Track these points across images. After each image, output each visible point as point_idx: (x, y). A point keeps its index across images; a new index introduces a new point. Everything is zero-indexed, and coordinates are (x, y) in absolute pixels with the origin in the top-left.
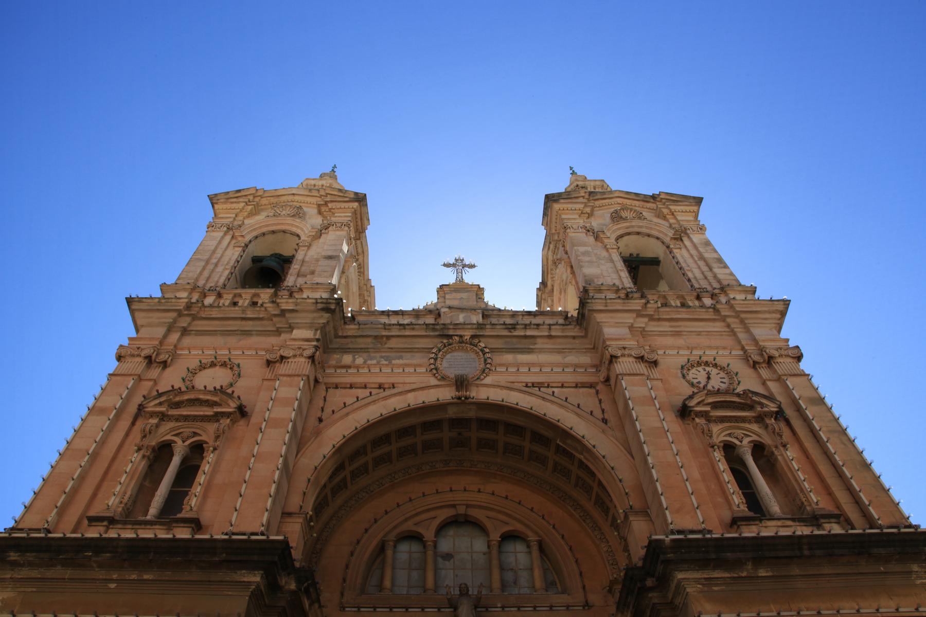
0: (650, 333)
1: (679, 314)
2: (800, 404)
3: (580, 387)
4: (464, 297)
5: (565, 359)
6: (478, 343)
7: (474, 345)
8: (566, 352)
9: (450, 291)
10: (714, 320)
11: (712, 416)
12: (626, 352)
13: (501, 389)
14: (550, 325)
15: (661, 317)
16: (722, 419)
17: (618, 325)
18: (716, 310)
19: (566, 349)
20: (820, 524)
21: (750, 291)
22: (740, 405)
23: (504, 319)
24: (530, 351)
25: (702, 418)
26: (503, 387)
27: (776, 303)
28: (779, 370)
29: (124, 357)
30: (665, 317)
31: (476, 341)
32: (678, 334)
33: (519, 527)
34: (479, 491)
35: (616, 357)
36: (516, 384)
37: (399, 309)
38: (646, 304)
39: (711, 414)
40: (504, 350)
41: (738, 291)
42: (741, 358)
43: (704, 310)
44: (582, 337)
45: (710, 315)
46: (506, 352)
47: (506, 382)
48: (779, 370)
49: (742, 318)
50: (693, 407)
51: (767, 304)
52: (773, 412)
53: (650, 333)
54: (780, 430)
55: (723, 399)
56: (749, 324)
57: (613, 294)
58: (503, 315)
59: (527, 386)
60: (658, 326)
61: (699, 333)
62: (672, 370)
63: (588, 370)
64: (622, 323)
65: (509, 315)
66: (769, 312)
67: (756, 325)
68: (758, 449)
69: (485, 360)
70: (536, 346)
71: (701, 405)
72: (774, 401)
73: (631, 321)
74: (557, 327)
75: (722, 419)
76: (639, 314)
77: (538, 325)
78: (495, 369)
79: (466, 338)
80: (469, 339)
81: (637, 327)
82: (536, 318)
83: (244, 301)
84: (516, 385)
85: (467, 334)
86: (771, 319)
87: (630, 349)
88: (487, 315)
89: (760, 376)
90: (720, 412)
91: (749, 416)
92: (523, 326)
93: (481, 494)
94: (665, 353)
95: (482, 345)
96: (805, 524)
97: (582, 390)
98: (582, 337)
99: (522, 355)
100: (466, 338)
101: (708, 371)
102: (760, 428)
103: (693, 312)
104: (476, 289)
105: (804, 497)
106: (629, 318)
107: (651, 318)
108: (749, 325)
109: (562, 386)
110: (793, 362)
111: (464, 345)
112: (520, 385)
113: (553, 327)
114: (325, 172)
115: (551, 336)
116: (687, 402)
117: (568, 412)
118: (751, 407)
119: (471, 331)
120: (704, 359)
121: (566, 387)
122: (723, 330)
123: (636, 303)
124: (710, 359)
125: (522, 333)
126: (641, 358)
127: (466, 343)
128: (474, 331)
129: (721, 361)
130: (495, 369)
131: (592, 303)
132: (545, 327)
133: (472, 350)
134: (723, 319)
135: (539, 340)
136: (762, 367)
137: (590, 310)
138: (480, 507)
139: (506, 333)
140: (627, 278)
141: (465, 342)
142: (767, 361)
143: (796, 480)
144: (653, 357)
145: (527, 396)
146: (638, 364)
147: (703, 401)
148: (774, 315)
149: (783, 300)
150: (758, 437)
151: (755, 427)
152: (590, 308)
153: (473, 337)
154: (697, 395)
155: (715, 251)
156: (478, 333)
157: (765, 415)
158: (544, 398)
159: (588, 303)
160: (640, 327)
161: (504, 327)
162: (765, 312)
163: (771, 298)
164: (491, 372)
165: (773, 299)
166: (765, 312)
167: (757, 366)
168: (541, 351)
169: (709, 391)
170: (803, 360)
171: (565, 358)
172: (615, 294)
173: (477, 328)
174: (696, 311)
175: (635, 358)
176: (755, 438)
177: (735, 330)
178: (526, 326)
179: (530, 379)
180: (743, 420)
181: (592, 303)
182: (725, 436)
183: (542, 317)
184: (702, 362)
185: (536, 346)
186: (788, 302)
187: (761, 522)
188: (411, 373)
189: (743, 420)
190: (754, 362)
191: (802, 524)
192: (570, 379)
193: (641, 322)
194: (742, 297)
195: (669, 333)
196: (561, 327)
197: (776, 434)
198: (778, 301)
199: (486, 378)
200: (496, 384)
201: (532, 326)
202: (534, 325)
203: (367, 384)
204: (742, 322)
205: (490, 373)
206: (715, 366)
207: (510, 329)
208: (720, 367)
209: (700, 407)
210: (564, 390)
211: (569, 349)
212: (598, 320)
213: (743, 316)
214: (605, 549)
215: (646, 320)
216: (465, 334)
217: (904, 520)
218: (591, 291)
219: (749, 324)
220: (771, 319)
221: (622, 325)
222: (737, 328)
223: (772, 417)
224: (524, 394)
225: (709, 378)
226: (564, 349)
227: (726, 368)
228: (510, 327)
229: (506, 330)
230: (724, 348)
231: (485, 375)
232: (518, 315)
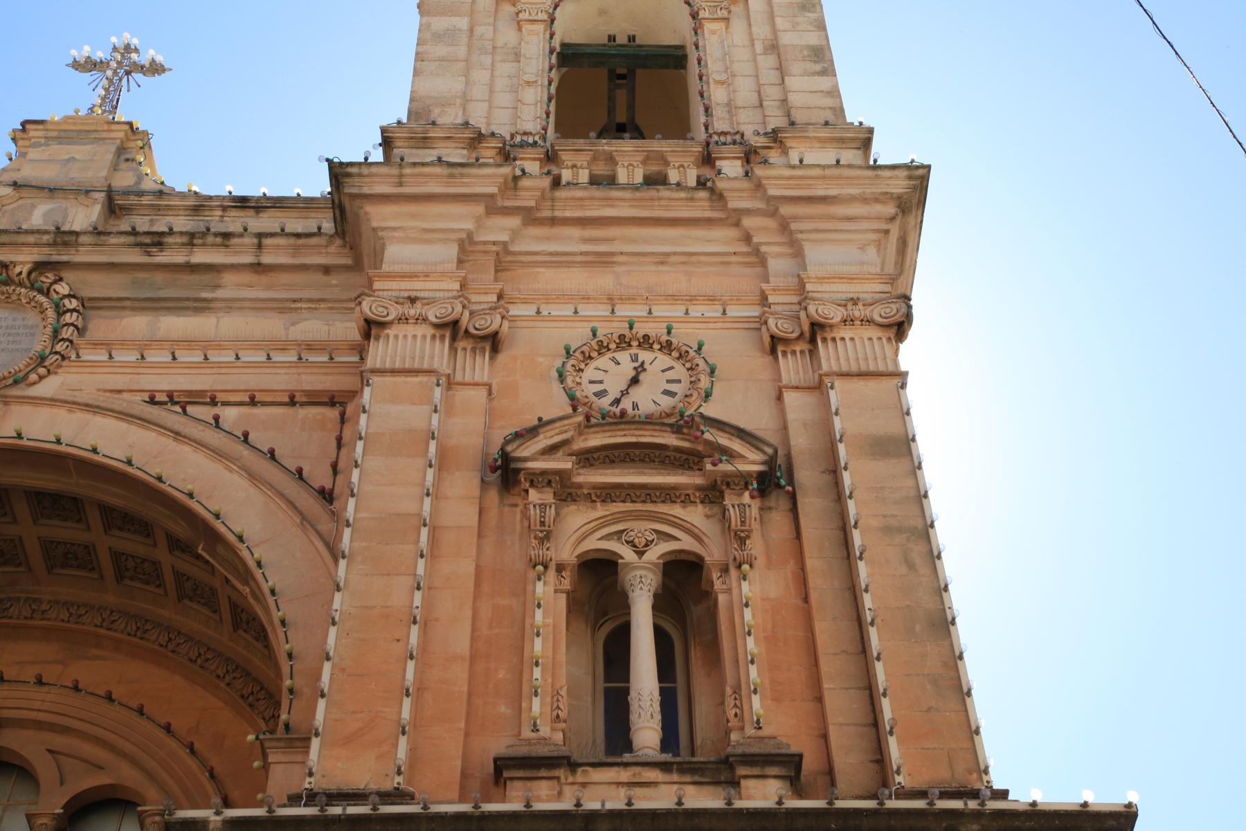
0: (523, 258)
1: (613, 206)
3: (303, 404)
4: (77, 157)
5: (292, 329)
6: (51, 284)
7: (40, 291)
8: (301, 309)
9: (45, 138)
10: (709, 222)
11: (580, 486)
12: (858, 312)
13: (70, 411)
14: (260, 236)
15: (558, 214)
16: (608, 493)
17: (428, 236)
18: (718, 197)
19: (301, 300)
20: (737, 779)
21: (852, 139)
22: (678, 455)
23: (171, 219)
24: (201, 306)
25: (548, 489)
26: (74, 403)
27: (887, 173)
29: (382, 325)
30: (568, 214)
31: (49, 278)
32: (603, 261)
33: (128, 776)
34: (40, 682)
36: (125, 395)
37: (293, 193)
38: (516, 179)
39: (579, 479)
40: (127, 303)
41: (820, 140)
42: (746, 325)
43: (683, 195)
44: (346, 268)
45: (701, 207)
46: (133, 309)
47: (98, 390)
49: (782, 216)
50: (525, 459)
51: (858, 178)
52: (749, 474)
53: (523, 258)
54: (743, 523)
55: (634, 440)
56: (801, 232)
57: (460, 151)
58: (169, 207)
59: (152, 401)
60: (548, 239)
61: (663, 259)
62: (541, 359)
63: (337, 359)
64: (443, 231)
65: (187, 208)
66: (864, 200)
67: (819, 236)
69: (56, 332)
70: (220, 293)
71: (560, 454)
72: (761, 445)
73: (469, 225)
74: (281, 241)
75: (608, 493)
76: (493, 207)
77: (227, 236)
78: (78, 356)
79: (18, 269)
80: (29, 273)
81: (485, 243)
82: (261, 215)
83: (630, 171)
84: (119, 403)
85: (23, 259)
86: (868, 218)
87: (430, 302)
88: (122, 208)
90: (605, 475)
91: (687, 486)
92: (185, 239)
93: (46, 689)
94: (538, 312)
95: (63, 289)
96: (697, 778)
97: (303, 412)
98: (346, 268)
99: (178, 316)
100: (18, 269)
101: (643, 363)
102: (707, 517)
103: (652, 199)
104: (121, 135)
105: (735, 705)
106: (462, 218)
107: (530, 217)
108: (800, 236)
109: (253, 402)
110: (880, 339)
111: (11, 289)
112: (138, 398)
113: (267, 241)
115: (259, 264)
116: (509, 448)
117: (231, 470)
118: (687, 460)
119: (35, 250)
120: (641, 329)
121: (264, 404)
122: (731, 250)
123: (489, 176)
124: (655, 330)
125: (180, 259)
126: (452, 329)
127: (21, 284)
128: (46, 250)
129: (685, 335)
130: (78, 356)
131: (360, 175)
132: (247, 240)
133: (33, 304)
134: (734, 219)
135: (228, 278)
136: (794, 352)
137: (354, 197)
138: (39, 725)
139: (135, 257)
141: (16, 279)
142: (807, 335)
145: (134, 428)
146: (438, 341)
147: (565, 443)
148: (878, 209)
149: (909, 167)
150: (695, 542)
151: (696, 515)
152: (354, 191)
153: (40, 267)
154: (549, 427)
155: (821, 26)
156: (55, 258)
157: (728, 484)
158: (177, 433)
159: (349, 175)
160: (494, 243)
161: (131, 239)
162: (852, 199)
163: (366, 159)
164: (65, 363)
165: (370, 160)
166: (852, 199)
167: (780, 349)
168: (231, 305)
169: (623, 413)
170: (913, 333)
171: (293, 324)
172: (465, 152)
173: (54, 244)
174: (660, 199)
175: (437, 326)
176: (686, 543)
177: (764, 249)
178: (192, 239)
179: (163, 383)
180: (669, 494)
181: (360, 175)
182: (607, 537)
183: (279, 214)
184: (635, 337)
185: (220, 293)
186: (921, 172)
187: (573, 772)
188: (227, 365)
189: (669, 494)
190: (772, 337)
191: (688, 778)
192: (281, 381)
193: (499, 230)
194: (827, 156)
195: (579, 258)
196: (292, 241)
197: (732, 534)
198: (894, 167)
199: (45, 381)
200: (68, 396)
201: (210, 239)
202: (216, 235)
203: (218, 394)
204: (784, 227)
205: (60, 366)
206: (667, 347)
207: (147, 245)
208: (679, 350)
209: (558, 460)
210: (258, 411)
211: (310, 300)
212: (375, 224)
213: (786, 210)
215: (514, 222)
216: (20, 258)
217: (975, 776)
218: (399, 143)
219: (801, 232)
220: (868, 218)
221: (441, 236)
222: (768, 244)
223: (746, 487)
224: (128, 422)
225: (635, 381)
226: (294, 301)
227: (692, 353)
228: (148, 240)
229: (137, 249)
230: (712, 299)
231: (42, 371)
232: (211, 208)
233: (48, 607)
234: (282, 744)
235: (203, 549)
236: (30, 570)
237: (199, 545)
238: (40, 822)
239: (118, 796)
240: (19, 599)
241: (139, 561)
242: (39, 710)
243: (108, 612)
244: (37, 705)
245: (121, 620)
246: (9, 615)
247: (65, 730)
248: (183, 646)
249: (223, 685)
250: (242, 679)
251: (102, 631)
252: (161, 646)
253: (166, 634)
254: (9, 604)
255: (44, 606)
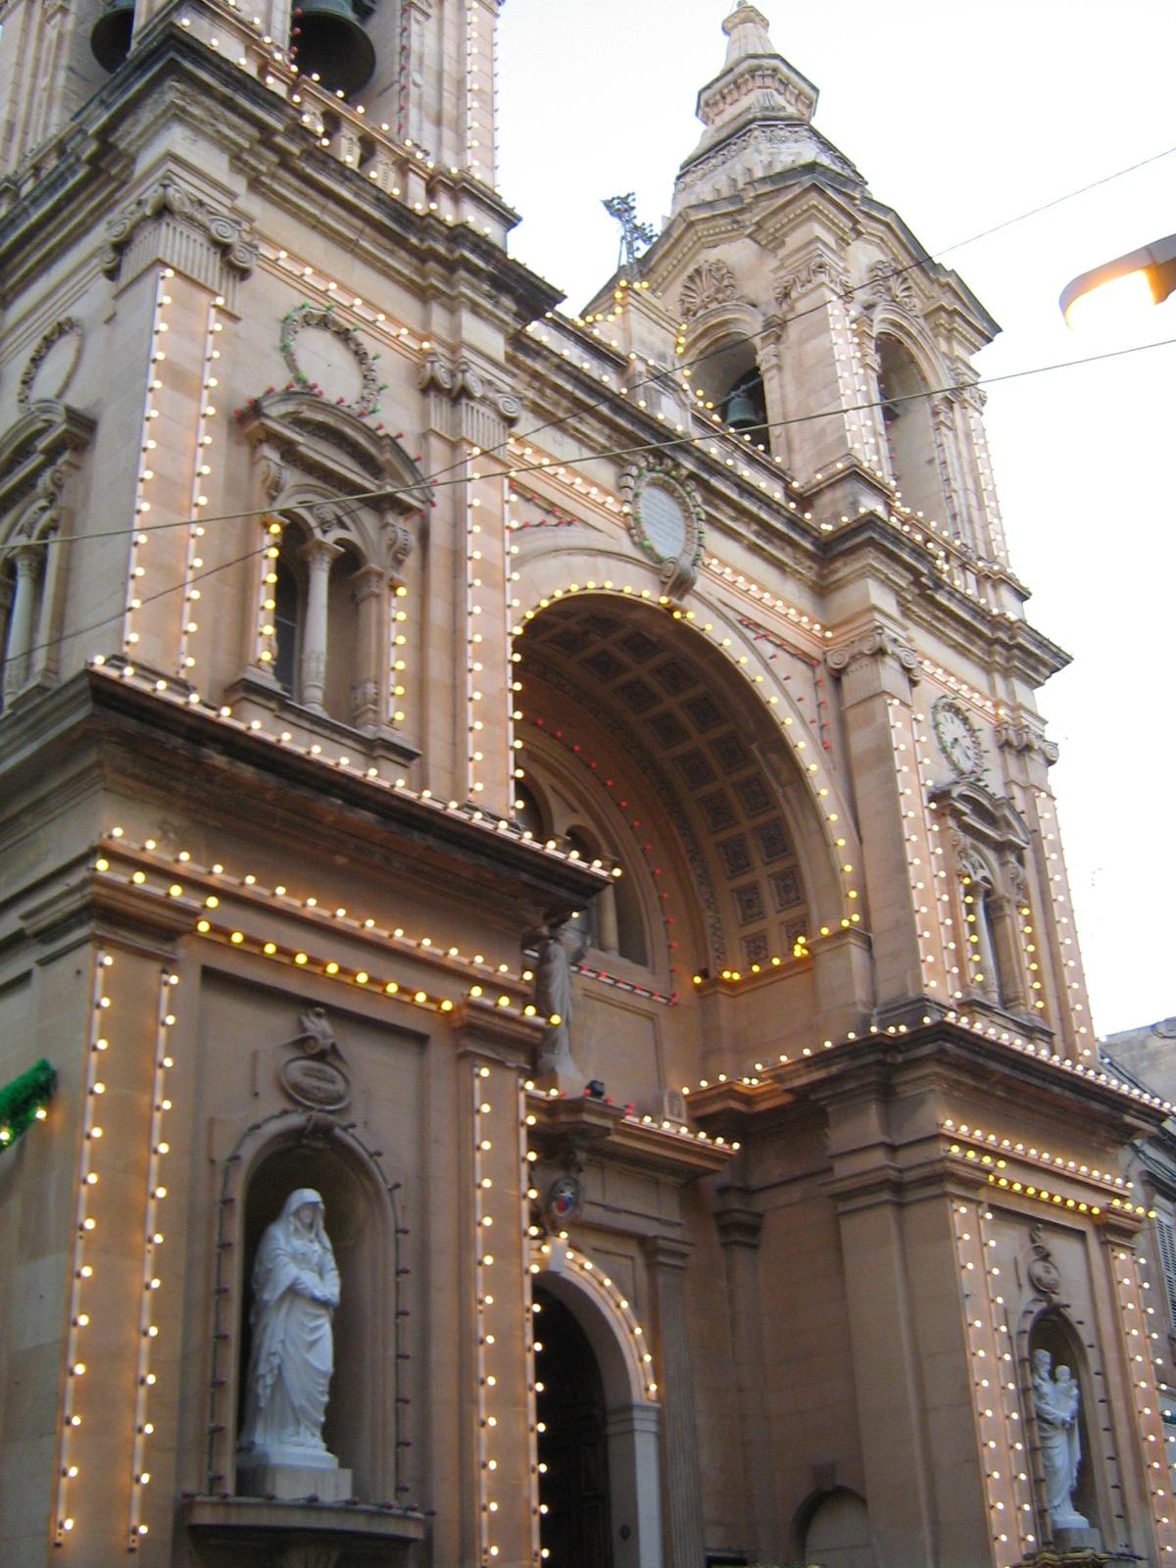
2: (466, 518)
12: (200, 216)
28: (166, 247)
35: (471, 397)
48: (166, 247)
59: (740, 622)
68: (348, 565)
89: (425, 417)
110: (201, 245)
114: (725, 17)
140: (285, 13)
143: (1013, 928)
144: (240, 256)
153: (692, 476)
214: (711, 921)
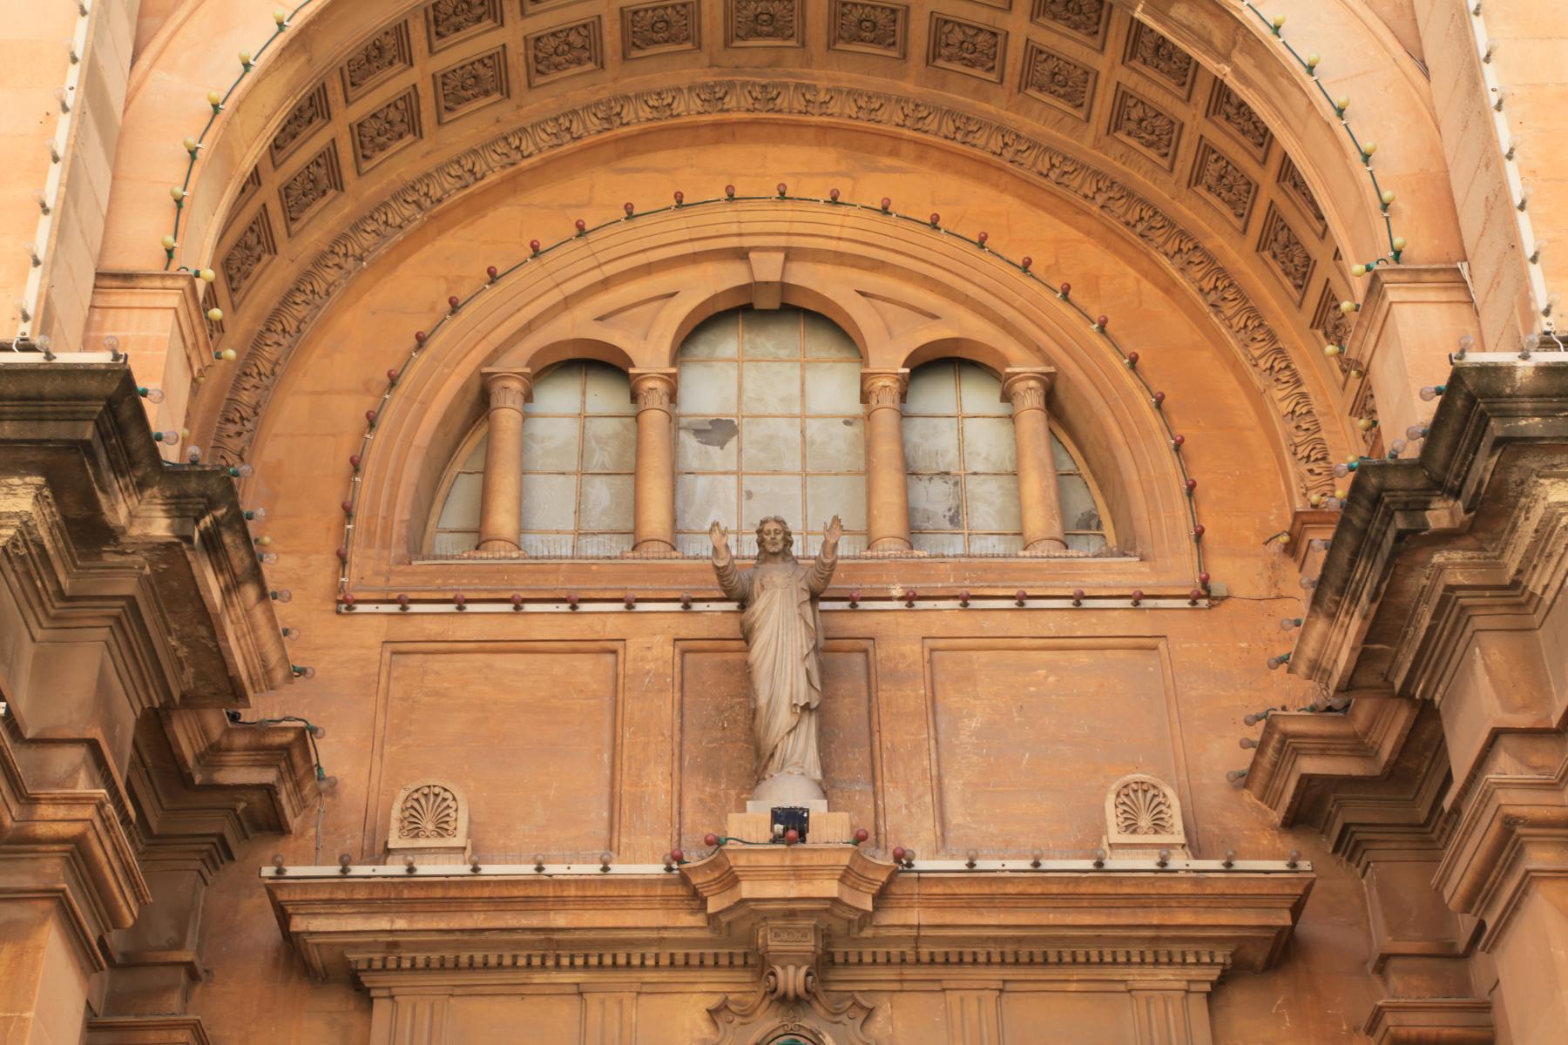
34: (834, 201)
93: (843, 209)
138: (839, 258)
233: (828, 98)
234: (1405, 277)
235: (1143, 11)
236: (803, 45)
237: (1137, 5)
238: (881, 384)
239: (959, 354)
240: (786, 86)
241: (972, 32)
242: (840, 239)
243: (912, 106)
244: (836, 232)
245: (931, 117)
246: (777, 108)
247: (878, 266)
248: (1025, 155)
249: (1095, 209)
250: (1123, 201)
251: (907, 133)
252: (994, 153)
253: (1000, 138)
254: (775, 92)
255: (823, 97)
